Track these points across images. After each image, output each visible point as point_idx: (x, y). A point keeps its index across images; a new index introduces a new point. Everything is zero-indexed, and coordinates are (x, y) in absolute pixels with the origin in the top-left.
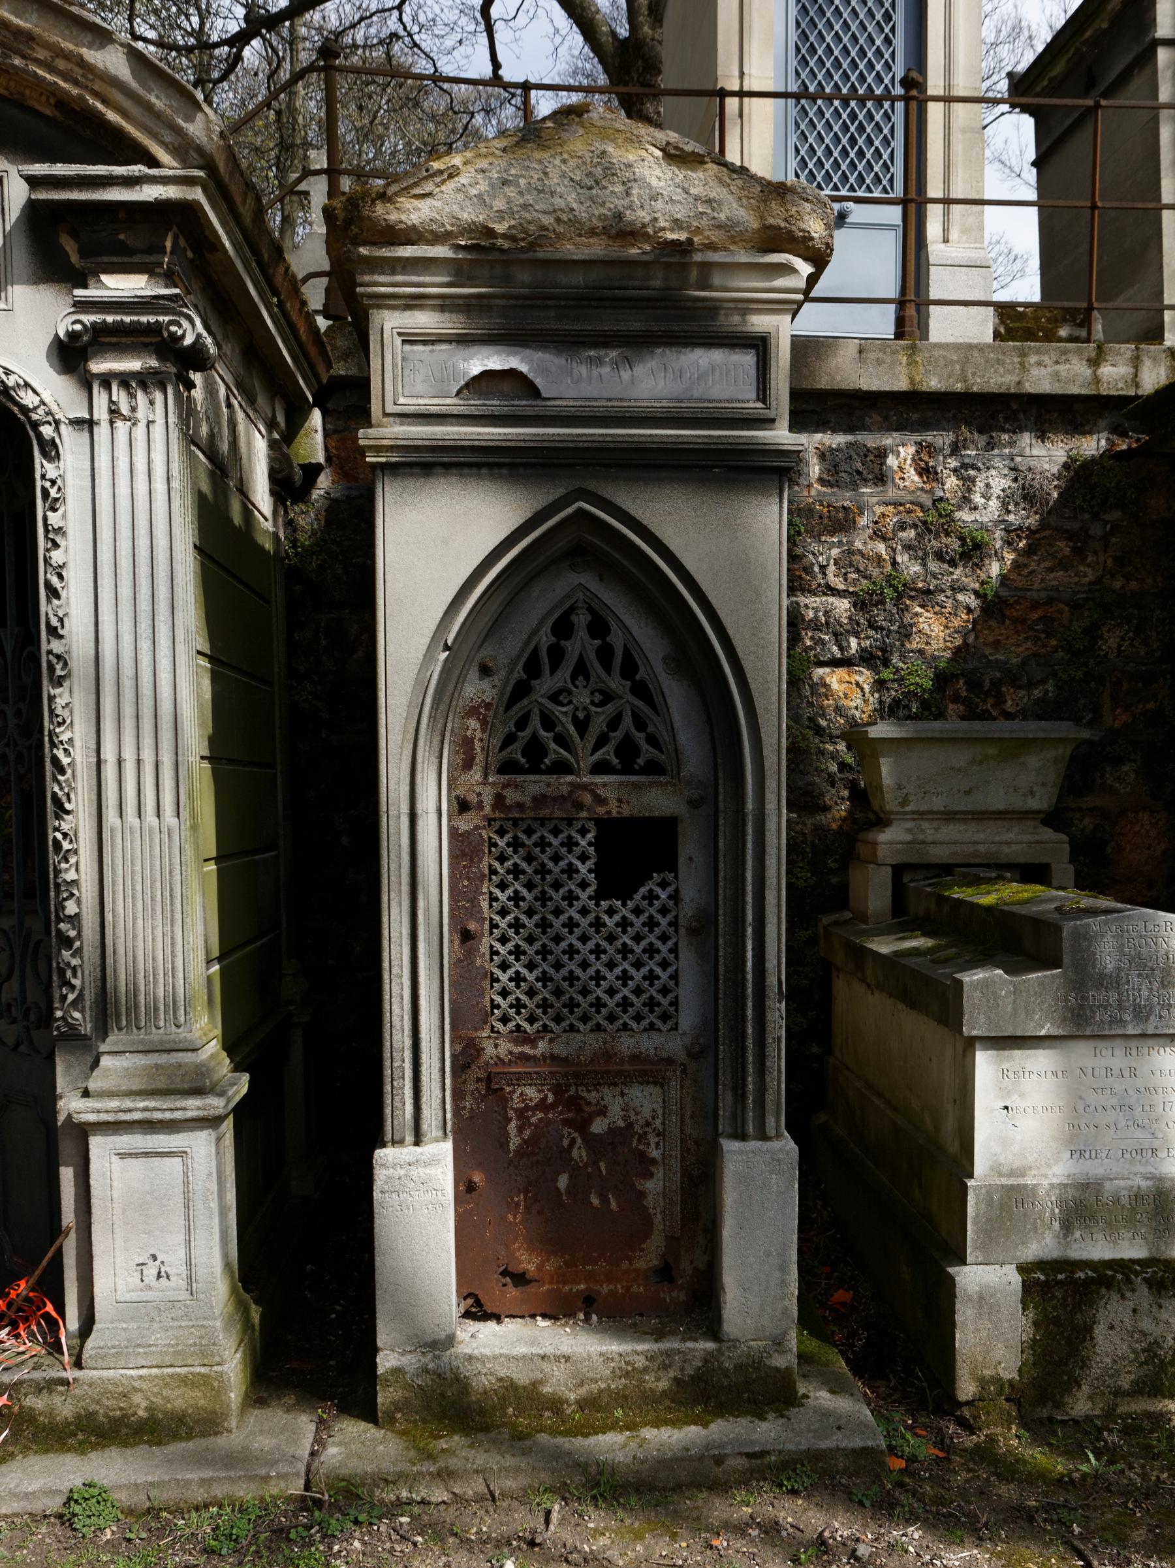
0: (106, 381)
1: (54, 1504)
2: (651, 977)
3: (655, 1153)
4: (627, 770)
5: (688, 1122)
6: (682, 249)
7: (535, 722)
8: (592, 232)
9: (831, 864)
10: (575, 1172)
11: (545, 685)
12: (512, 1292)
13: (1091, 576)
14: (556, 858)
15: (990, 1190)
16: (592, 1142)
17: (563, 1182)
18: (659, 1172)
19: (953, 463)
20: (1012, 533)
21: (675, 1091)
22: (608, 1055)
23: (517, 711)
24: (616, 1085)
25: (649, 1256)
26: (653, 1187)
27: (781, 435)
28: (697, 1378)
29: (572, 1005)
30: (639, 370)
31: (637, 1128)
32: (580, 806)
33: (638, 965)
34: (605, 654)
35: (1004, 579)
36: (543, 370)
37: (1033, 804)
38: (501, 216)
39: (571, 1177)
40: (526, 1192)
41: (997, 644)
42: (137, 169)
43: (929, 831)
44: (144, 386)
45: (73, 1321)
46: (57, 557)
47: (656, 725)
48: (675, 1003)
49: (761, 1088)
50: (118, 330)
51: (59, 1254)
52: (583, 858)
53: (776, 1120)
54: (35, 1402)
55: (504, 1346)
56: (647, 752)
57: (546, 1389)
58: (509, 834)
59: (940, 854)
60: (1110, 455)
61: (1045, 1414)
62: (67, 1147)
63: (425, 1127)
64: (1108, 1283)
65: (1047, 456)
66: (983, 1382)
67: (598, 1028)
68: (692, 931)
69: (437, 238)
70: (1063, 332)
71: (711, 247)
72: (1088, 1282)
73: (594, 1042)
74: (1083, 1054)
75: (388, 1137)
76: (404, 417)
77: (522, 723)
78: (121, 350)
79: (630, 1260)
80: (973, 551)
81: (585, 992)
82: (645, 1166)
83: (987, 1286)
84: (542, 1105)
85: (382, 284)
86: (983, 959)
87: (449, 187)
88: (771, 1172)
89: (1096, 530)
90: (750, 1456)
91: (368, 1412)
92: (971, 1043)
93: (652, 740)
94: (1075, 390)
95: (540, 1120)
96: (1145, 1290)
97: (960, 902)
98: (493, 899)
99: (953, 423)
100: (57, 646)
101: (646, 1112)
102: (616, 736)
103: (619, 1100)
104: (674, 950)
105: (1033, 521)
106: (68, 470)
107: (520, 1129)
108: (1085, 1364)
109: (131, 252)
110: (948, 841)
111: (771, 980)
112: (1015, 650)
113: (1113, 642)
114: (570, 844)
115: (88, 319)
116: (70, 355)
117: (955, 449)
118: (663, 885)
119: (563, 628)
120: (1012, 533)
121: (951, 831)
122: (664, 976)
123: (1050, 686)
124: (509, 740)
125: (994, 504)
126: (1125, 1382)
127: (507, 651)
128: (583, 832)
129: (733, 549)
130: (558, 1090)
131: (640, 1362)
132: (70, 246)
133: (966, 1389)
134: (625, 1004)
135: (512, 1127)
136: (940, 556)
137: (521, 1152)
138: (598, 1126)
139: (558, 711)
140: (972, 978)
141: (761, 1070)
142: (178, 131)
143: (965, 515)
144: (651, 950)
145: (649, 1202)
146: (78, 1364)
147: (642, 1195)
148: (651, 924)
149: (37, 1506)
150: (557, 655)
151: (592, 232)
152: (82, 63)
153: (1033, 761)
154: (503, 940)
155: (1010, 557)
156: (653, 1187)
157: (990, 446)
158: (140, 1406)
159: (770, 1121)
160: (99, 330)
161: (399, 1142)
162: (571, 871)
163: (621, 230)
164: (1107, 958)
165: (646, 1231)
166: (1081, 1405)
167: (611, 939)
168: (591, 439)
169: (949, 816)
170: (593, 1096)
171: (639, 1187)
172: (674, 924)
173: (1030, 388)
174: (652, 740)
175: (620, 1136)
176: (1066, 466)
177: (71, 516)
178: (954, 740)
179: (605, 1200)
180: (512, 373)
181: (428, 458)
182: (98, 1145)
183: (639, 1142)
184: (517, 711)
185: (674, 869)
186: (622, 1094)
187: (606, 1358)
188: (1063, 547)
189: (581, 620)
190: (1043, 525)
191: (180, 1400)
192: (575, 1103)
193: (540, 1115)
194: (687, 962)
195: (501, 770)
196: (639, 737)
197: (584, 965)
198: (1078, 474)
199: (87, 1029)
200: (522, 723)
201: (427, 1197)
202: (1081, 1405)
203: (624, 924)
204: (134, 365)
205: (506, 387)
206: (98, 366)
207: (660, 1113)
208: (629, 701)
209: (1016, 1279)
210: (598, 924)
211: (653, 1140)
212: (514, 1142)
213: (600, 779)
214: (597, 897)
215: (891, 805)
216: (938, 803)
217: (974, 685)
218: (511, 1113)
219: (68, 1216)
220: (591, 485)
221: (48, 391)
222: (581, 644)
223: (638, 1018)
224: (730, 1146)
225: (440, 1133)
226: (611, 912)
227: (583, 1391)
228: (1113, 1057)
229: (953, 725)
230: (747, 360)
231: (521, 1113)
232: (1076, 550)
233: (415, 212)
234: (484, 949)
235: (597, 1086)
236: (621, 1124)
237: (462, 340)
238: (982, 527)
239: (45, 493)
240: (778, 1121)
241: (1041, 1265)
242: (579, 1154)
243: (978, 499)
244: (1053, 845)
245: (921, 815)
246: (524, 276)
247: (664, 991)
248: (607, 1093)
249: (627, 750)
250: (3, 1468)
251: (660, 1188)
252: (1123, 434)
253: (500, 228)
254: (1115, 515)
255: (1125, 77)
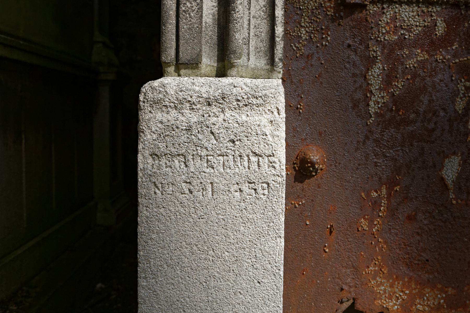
39: (464, 162)
40: (391, 184)
63: (239, 37)
75: (169, 54)
95: (422, 64)
107: (388, 79)
161: (190, 65)
193: (421, 56)
201: (241, 169)
212: (377, 100)
218: (376, 50)
225: (262, 63)
231: (391, 51)
250: (142, 308)
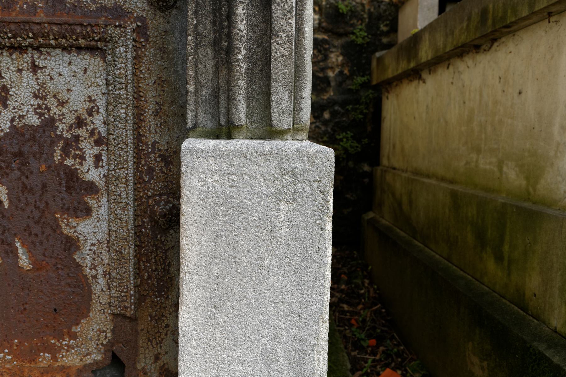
3: (93, 174)
5: (151, 122)
9: (384, 28)
18: (101, 207)
24: (21, 49)
31: (61, 127)
79: (54, 351)
82: (77, 194)
88: (278, 197)
101: (77, 103)
103: (28, 78)
145: (84, 257)
147: (71, 244)
159: (281, 97)
165: (81, 306)
171: (67, 231)
183: (66, 152)
186: (35, 68)
207: (101, 104)
211: (89, 150)
236: (34, 120)
240: (296, 100)
251: (102, 236)
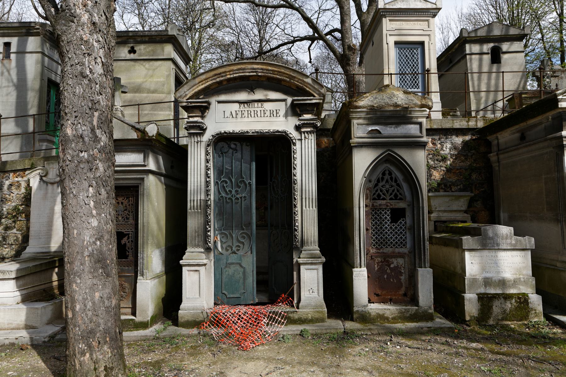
0: (304, 132)
1: (299, 332)
2: (401, 238)
3: (403, 271)
4: (396, 199)
6: (407, 108)
7: (379, 191)
8: (391, 106)
10: (388, 274)
11: (381, 184)
12: (376, 298)
13: (469, 164)
14: (383, 216)
15: (470, 279)
16: (391, 269)
17: (385, 276)
18: (404, 275)
19: (439, 142)
20: (452, 156)
21: (406, 260)
22: (394, 252)
23: (376, 189)
25: (402, 292)
26: (403, 278)
27: (425, 139)
28: (414, 314)
29: (387, 243)
30: (398, 129)
32: (387, 206)
33: (399, 235)
34: (391, 178)
35: (451, 164)
36: (382, 129)
37: (462, 209)
38: (375, 104)
41: (450, 177)
42: (312, 98)
43: (441, 214)
44: (310, 133)
45: (295, 301)
46: (295, 162)
47: (401, 191)
48: (406, 243)
49: (425, 258)
50: (307, 124)
51: (293, 288)
52: (388, 216)
53: (427, 265)
54: (291, 315)
55: (375, 308)
56: (400, 196)
57: (386, 315)
58: (373, 212)
59: (443, 219)
60: (471, 139)
61: (484, 323)
62: (295, 268)
64: (495, 297)
65: (459, 140)
66: (471, 317)
67: (391, 247)
68: (409, 229)
69: (364, 107)
70: (451, 114)
71: (412, 108)
72: (491, 297)
73: (391, 250)
74: (486, 253)
76: (357, 137)
77: (377, 191)
78: (307, 127)
80: (444, 159)
81: (389, 240)
83: (470, 297)
84: (381, 262)
85: (354, 115)
86: (464, 235)
87: (366, 99)
89: (469, 154)
90: (428, 328)
91: (352, 320)
92: (464, 250)
93: (400, 194)
94: (464, 127)
96: (503, 299)
97: (452, 227)
98: (372, 223)
99: (439, 134)
100: (295, 178)
101: (401, 263)
102: (394, 193)
104: (405, 233)
105: (456, 153)
106: (297, 147)
108: (491, 314)
109: (308, 111)
110: (445, 216)
111: (426, 238)
112: (454, 179)
113: (474, 177)
114: (386, 213)
115: (302, 122)
116: (298, 128)
117: (439, 139)
118: (403, 220)
119: (384, 174)
120: (452, 156)
121: (445, 214)
122: (404, 237)
123: (461, 186)
124: (374, 194)
125: (448, 150)
126: (500, 317)
127: (374, 178)
128: (388, 211)
129: (418, 160)
130: (384, 259)
131: (403, 311)
132: (298, 110)
133: (468, 318)
134: (396, 243)
135: (376, 266)
136: (437, 160)
137: (378, 271)
138: (392, 266)
139: (383, 189)
140: (464, 238)
141: (424, 255)
142: (319, 91)
143: (442, 152)
144: (401, 233)
145: (402, 281)
146: (298, 308)
147: (401, 279)
148: (401, 228)
149: (296, 332)
150: (383, 179)
151: (391, 106)
152: (303, 81)
153: (462, 200)
154: (374, 231)
155: (452, 160)
156: (403, 278)
157: (447, 138)
158: (310, 317)
159: (427, 264)
160: (303, 124)
161: (357, 267)
162: (386, 218)
163: (396, 105)
164: (490, 234)
166: (491, 322)
167: (394, 230)
168: (391, 141)
169: (445, 211)
170: (391, 260)
172: (405, 228)
173: (455, 127)
174: (400, 194)
175: (397, 268)
176: (462, 142)
177: (298, 156)
178: (446, 196)
179: (393, 280)
180: (376, 130)
181: (362, 144)
182: (302, 267)
184: (376, 189)
185: (405, 217)
187: (397, 310)
188: (463, 158)
189: (387, 172)
190: (458, 154)
191: (317, 316)
192: (388, 261)
194: (408, 235)
195: (373, 200)
196: (398, 193)
197: (389, 235)
198: (465, 143)
199: (299, 246)
200: (377, 191)
202: (491, 322)
203: (396, 228)
204: (309, 130)
205: (375, 132)
206: (303, 130)
208: (396, 187)
209: (477, 296)
210: (391, 228)
212: (376, 269)
213: (391, 201)
214: (391, 223)
215: (433, 209)
216: (442, 209)
217: (446, 186)
219: (295, 281)
220: (390, 149)
221: (294, 134)
222: (387, 177)
223: (399, 245)
224: (419, 269)
226: (393, 225)
227: (393, 316)
228: (492, 253)
229: (442, 193)
230: (418, 126)
232: (465, 159)
233: (361, 103)
234: (370, 232)
235: (392, 258)
237: (368, 125)
238: (446, 154)
239: (294, 152)
241: (481, 294)
242: (388, 271)
243: (444, 149)
244: (467, 216)
245: (439, 211)
246: (379, 113)
247: (404, 240)
248: (393, 259)
249: (396, 196)
252: (474, 135)
253: (375, 106)
254: (473, 151)
255: (459, 61)
